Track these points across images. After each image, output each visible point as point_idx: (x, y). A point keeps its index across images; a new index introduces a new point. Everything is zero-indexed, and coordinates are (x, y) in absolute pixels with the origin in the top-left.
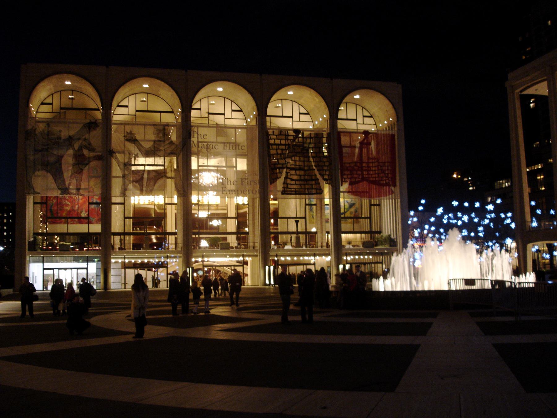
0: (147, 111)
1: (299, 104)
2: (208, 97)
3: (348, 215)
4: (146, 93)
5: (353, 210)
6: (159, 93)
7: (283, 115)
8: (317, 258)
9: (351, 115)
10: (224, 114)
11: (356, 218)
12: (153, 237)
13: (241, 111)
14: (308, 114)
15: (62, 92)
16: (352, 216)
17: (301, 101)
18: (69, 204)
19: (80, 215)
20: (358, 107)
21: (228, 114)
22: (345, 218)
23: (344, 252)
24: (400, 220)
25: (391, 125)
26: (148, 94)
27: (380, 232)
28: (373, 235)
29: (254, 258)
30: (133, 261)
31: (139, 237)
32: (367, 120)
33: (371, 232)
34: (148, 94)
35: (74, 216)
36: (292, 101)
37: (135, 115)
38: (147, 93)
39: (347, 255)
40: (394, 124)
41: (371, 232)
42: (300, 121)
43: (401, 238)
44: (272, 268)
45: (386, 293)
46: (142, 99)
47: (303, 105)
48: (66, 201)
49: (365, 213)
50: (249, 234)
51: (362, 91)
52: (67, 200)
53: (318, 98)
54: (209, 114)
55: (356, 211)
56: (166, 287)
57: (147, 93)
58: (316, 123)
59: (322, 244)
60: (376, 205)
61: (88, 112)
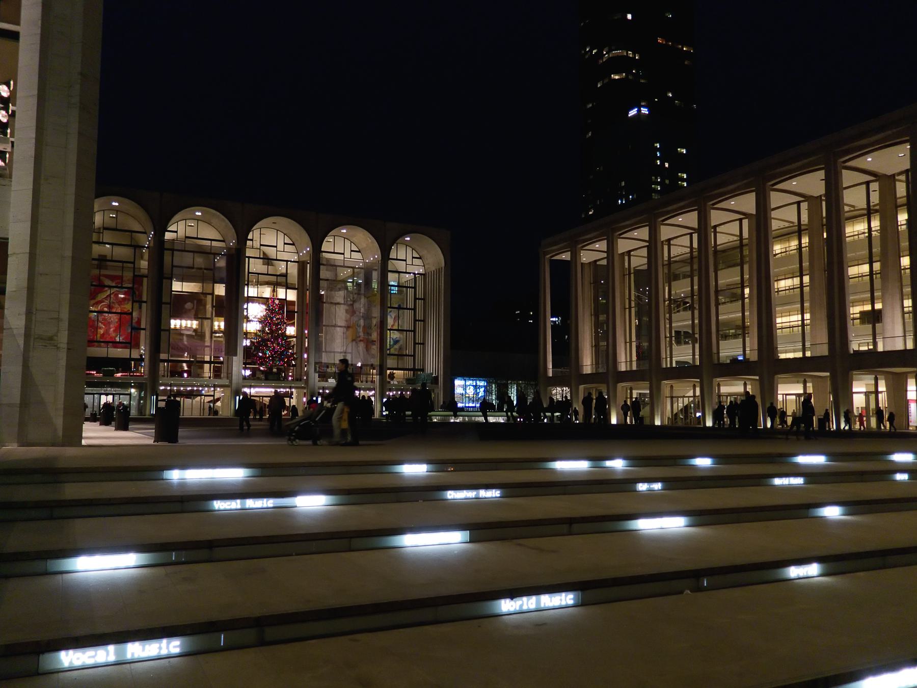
0: (197, 238)
1: (285, 234)
2: (260, 228)
3: (392, 351)
4: (198, 219)
5: (397, 347)
6: (212, 221)
7: (335, 251)
8: (252, 389)
9: (401, 256)
10: (276, 247)
11: (400, 356)
12: (185, 365)
13: (293, 244)
14: (359, 252)
15: (187, 221)
16: (397, 353)
17: (354, 239)
18: (103, 327)
19: (115, 339)
20: (347, 242)
21: (280, 247)
22: (390, 355)
23: (388, 387)
24: (442, 360)
25: (439, 269)
26: (199, 221)
27: (423, 370)
28: (415, 372)
29: (226, 388)
30: (189, 389)
31: (174, 363)
32: (416, 261)
33: (414, 370)
34: (199, 221)
35: (108, 340)
36: (345, 238)
37: (260, 249)
38: (186, 220)
39: (390, 390)
40: (442, 268)
41: (414, 370)
42: (412, 265)
43: (442, 377)
44: (155, 397)
45: (178, 431)
46: (111, 215)
47: (355, 243)
48: (100, 324)
49: (409, 351)
50: (223, 364)
51: (412, 235)
52: (102, 323)
53: (370, 239)
54: (261, 245)
55: (400, 348)
56: (199, 415)
57: (198, 220)
58: (301, 254)
59: (366, 378)
60: (420, 344)
61: (134, 234)
